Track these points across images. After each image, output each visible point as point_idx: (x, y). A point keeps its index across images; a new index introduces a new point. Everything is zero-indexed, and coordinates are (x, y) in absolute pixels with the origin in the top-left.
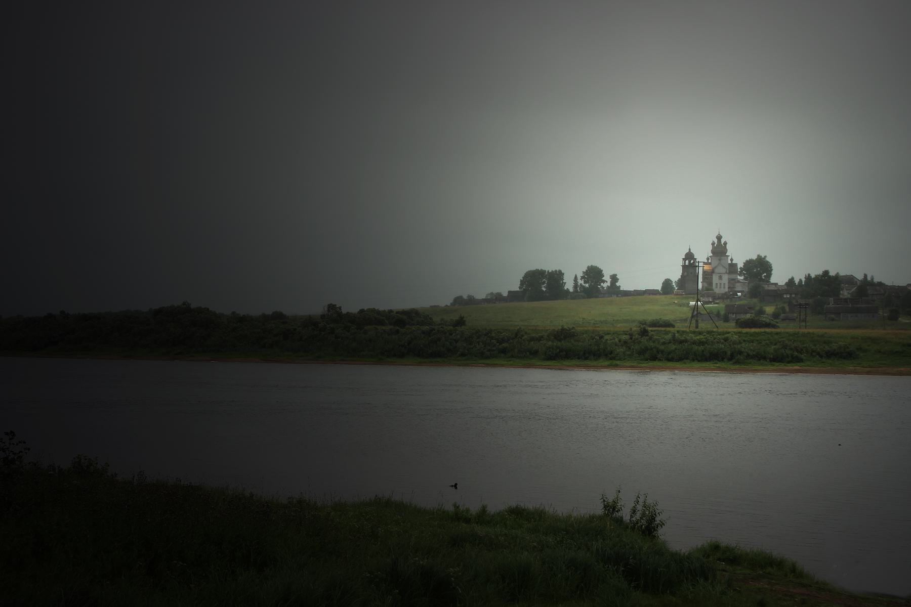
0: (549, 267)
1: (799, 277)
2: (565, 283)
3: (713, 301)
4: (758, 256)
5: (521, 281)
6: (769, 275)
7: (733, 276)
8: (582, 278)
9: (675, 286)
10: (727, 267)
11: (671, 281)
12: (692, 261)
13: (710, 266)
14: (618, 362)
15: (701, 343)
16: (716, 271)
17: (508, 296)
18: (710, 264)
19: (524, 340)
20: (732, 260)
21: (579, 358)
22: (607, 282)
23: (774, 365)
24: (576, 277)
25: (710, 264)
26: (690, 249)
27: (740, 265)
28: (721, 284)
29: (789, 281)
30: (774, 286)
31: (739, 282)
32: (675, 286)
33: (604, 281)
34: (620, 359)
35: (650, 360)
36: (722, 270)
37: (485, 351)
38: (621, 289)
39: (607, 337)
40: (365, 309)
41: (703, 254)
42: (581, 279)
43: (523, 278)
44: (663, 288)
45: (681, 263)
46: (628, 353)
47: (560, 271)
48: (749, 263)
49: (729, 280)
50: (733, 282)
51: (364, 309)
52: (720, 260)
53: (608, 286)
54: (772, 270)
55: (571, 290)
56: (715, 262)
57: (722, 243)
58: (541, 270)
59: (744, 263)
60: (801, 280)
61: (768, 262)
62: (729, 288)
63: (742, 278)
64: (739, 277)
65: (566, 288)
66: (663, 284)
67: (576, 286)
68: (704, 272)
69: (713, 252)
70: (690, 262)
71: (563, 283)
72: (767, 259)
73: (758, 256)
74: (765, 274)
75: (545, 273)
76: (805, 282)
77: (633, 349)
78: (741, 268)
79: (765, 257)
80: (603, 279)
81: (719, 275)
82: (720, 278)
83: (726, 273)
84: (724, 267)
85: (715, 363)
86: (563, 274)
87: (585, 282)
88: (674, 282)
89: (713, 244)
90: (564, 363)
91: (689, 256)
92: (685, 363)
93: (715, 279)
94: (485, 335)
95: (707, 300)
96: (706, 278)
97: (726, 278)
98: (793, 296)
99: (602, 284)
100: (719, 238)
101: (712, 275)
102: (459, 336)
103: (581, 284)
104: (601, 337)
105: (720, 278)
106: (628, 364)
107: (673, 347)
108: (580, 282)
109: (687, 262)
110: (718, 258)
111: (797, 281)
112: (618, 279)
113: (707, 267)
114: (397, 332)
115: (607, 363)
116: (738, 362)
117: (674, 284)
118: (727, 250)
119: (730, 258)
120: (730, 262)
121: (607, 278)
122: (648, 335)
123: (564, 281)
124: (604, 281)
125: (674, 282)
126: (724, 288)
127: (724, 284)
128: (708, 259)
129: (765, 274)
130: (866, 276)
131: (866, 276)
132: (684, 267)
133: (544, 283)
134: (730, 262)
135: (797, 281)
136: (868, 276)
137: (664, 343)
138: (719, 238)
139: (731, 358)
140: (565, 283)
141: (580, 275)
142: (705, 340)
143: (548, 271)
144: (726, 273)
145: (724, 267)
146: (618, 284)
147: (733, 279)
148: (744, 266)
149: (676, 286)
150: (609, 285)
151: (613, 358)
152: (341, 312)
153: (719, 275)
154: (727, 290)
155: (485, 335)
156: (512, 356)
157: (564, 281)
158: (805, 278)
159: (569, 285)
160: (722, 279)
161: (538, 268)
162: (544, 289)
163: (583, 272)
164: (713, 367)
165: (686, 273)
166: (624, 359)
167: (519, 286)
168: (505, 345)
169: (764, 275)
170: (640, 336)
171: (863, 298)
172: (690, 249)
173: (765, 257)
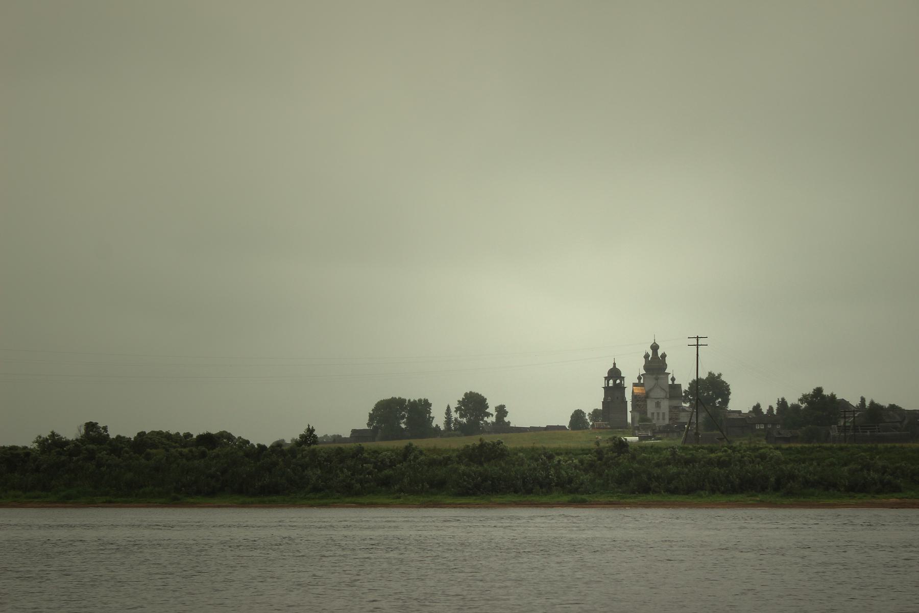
0: (411, 394)
1: (768, 403)
2: (433, 418)
3: (653, 436)
4: (710, 373)
5: (370, 415)
6: (726, 401)
7: (675, 403)
8: (457, 409)
9: (589, 421)
10: (667, 390)
11: (583, 413)
12: (618, 381)
13: (643, 388)
14: (585, 497)
15: (721, 464)
16: (652, 394)
17: (351, 437)
18: (642, 385)
19: (419, 464)
20: (673, 379)
21: (516, 492)
22: (492, 415)
23: (855, 497)
24: (448, 409)
25: (642, 385)
26: (615, 364)
27: (685, 387)
28: (658, 414)
29: (753, 409)
30: (738, 415)
31: (684, 410)
32: (589, 421)
33: (488, 415)
34: (587, 492)
35: (639, 493)
36: (662, 394)
37: (353, 482)
38: (511, 425)
39: (557, 458)
40: (147, 433)
41: (633, 370)
42: (456, 411)
43: (373, 410)
44: (571, 423)
45: (603, 383)
46: (598, 481)
47: (426, 401)
48: (697, 384)
49: (670, 408)
50: (675, 410)
51: (145, 432)
52: (657, 379)
53: (493, 423)
54: (729, 393)
55: (442, 427)
56: (651, 383)
57: (659, 356)
58: (400, 398)
59: (690, 384)
60: (771, 408)
61: (724, 382)
62: (670, 419)
63: (688, 405)
64: (684, 405)
65: (434, 425)
66: (572, 417)
67: (448, 421)
68: (635, 397)
69: (646, 368)
70: (615, 382)
71: (430, 417)
72: (723, 378)
73: (710, 373)
74: (720, 400)
75: (406, 402)
76: (778, 409)
77: (608, 475)
78: (686, 391)
79: (720, 375)
80: (487, 411)
81: (656, 401)
82: (658, 405)
83: (666, 398)
84: (664, 390)
85: (751, 496)
86: (430, 405)
87: (461, 416)
88: (587, 414)
89: (646, 356)
90: (493, 499)
91: (614, 373)
92: (701, 496)
93: (651, 406)
94: (353, 457)
95: (643, 433)
96: (638, 405)
97: (665, 405)
98: (770, 426)
99: (486, 419)
100: (655, 348)
101: (646, 401)
102: (307, 459)
103: (456, 419)
104: (550, 457)
105: (658, 405)
106: (602, 499)
107: (673, 469)
108: (455, 415)
109: (611, 382)
110: (654, 376)
111: (765, 410)
112: (507, 412)
113: (638, 390)
114: (203, 455)
115: (566, 498)
116: (790, 493)
117: (587, 417)
118: (667, 365)
119: (670, 377)
120: (670, 382)
121: (491, 409)
122: (627, 451)
123: (432, 415)
124: (488, 415)
125: (587, 414)
126: (664, 419)
127: (664, 414)
128: (639, 378)
129: (720, 400)
130: (863, 400)
131: (863, 400)
132: (607, 389)
133: (403, 417)
134: (670, 382)
135: (765, 410)
136: (866, 400)
137: (658, 465)
138: (655, 348)
139: (778, 487)
140: (433, 418)
141: (454, 405)
142: (727, 459)
143: (409, 400)
144: (666, 398)
145: (664, 390)
146: (506, 419)
147: (676, 407)
148: (689, 388)
149: (591, 421)
150: (494, 421)
151: (575, 491)
152: (108, 435)
153: (656, 401)
154: (667, 422)
155: (353, 457)
156: (401, 490)
157: (432, 415)
158: (778, 404)
159: (439, 420)
160: (660, 407)
161: (394, 396)
162: (403, 426)
163: (459, 401)
164: (750, 502)
165: (609, 398)
166: (594, 492)
167: (367, 421)
168: (387, 472)
169: (717, 401)
170: (616, 454)
171: (881, 424)
172: (615, 364)
173: (720, 375)
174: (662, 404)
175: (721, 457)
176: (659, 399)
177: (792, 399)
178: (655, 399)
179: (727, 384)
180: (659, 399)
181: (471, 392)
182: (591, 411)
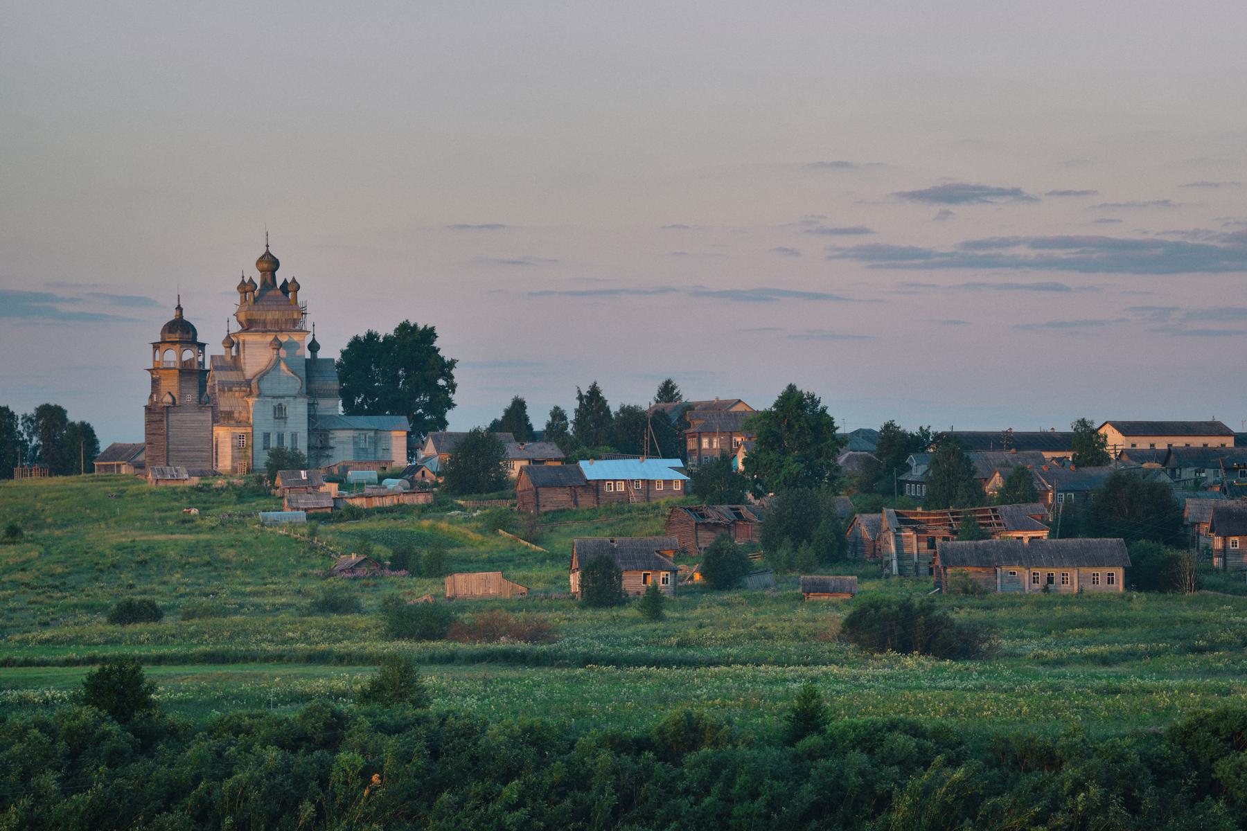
11: (12, 415)
60: (558, 414)
81: (276, 402)
88: (20, 417)
100: (269, 264)
120: (308, 355)
138: (269, 264)
153: (276, 402)
160: (286, 418)
172: (179, 308)
174: (290, 411)
175: (120, 784)
176: (283, 397)
177: (608, 404)
178: (274, 397)
179: (453, 387)
180: (283, 397)
181: (89, 425)
182: (31, 411)
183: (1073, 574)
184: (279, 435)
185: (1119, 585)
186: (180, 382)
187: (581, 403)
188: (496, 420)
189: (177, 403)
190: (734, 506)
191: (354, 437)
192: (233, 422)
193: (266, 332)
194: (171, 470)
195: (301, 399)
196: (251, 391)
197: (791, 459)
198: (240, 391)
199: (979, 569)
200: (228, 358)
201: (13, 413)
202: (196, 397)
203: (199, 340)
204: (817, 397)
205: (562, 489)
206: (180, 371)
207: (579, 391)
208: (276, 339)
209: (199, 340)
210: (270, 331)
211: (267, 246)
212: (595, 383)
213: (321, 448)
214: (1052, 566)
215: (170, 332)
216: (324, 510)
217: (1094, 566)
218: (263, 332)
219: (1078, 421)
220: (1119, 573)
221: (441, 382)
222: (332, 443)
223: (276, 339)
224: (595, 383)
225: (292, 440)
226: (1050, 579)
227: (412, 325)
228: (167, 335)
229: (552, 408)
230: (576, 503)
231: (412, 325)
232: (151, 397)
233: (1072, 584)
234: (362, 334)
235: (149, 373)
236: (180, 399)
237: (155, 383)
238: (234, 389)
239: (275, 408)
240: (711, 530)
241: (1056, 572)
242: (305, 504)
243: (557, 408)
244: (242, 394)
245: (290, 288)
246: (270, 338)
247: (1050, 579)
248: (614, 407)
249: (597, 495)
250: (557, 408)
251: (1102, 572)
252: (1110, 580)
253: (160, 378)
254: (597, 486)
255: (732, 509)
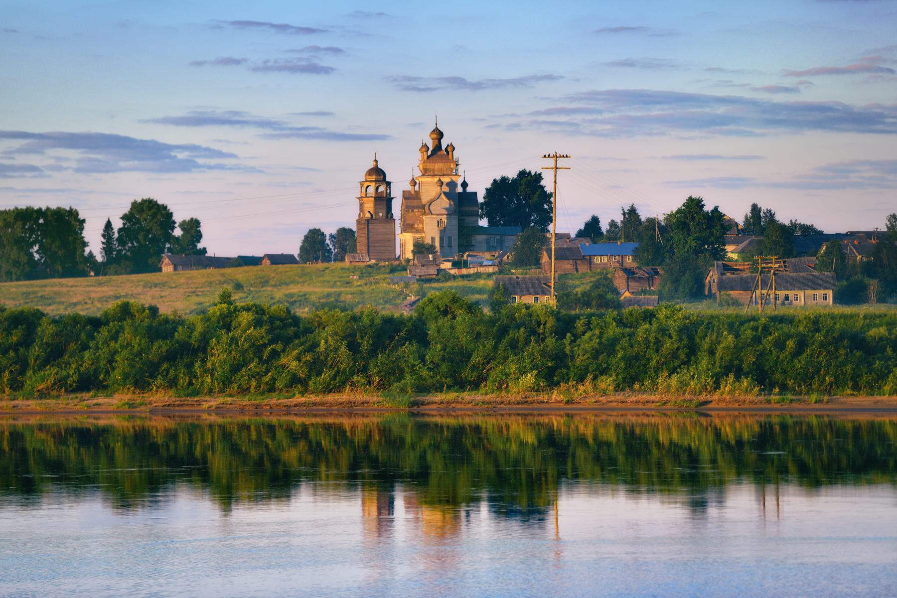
11: (323, 234)
100: (439, 134)
172: (376, 161)
183: (801, 294)
184: (449, 238)
185: (830, 300)
186: (376, 205)
187: (624, 217)
188: (580, 229)
189: (374, 218)
190: (654, 267)
191: (487, 239)
192: (414, 231)
193: (434, 175)
194: (359, 256)
195: (454, 216)
196: (425, 212)
197: (692, 238)
198: (418, 212)
199: (742, 292)
200: (413, 192)
201: (323, 233)
202: (385, 214)
203: (388, 179)
204: (773, 212)
205: (568, 261)
206: (375, 198)
207: (623, 210)
208: (440, 180)
209: (388, 179)
210: (436, 175)
211: (436, 124)
212: (633, 205)
213: (466, 246)
214: (787, 289)
215: (369, 175)
216: (431, 276)
217: (814, 289)
218: (432, 176)
219: (891, 216)
220: (830, 293)
221: (546, 206)
222: (473, 243)
223: (440, 180)
224: (633, 205)
225: (449, 241)
226: (787, 298)
227: (528, 172)
228: (368, 177)
229: (610, 221)
230: (577, 270)
231: (528, 172)
232: (360, 214)
233: (800, 301)
234: (498, 178)
235: (358, 200)
236: (375, 215)
237: (362, 205)
238: (415, 210)
239: (438, 221)
240: (637, 282)
241: (791, 293)
242: (420, 272)
243: (613, 221)
244: (419, 213)
245: (451, 148)
246: (436, 179)
247: (787, 298)
248: (643, 218)
249: (590, 264)
250: (613, 221)
251: (820, 292)
252: (825, 298)
253: (364, 203)
254: (590, 259)
255: (652, 269)
